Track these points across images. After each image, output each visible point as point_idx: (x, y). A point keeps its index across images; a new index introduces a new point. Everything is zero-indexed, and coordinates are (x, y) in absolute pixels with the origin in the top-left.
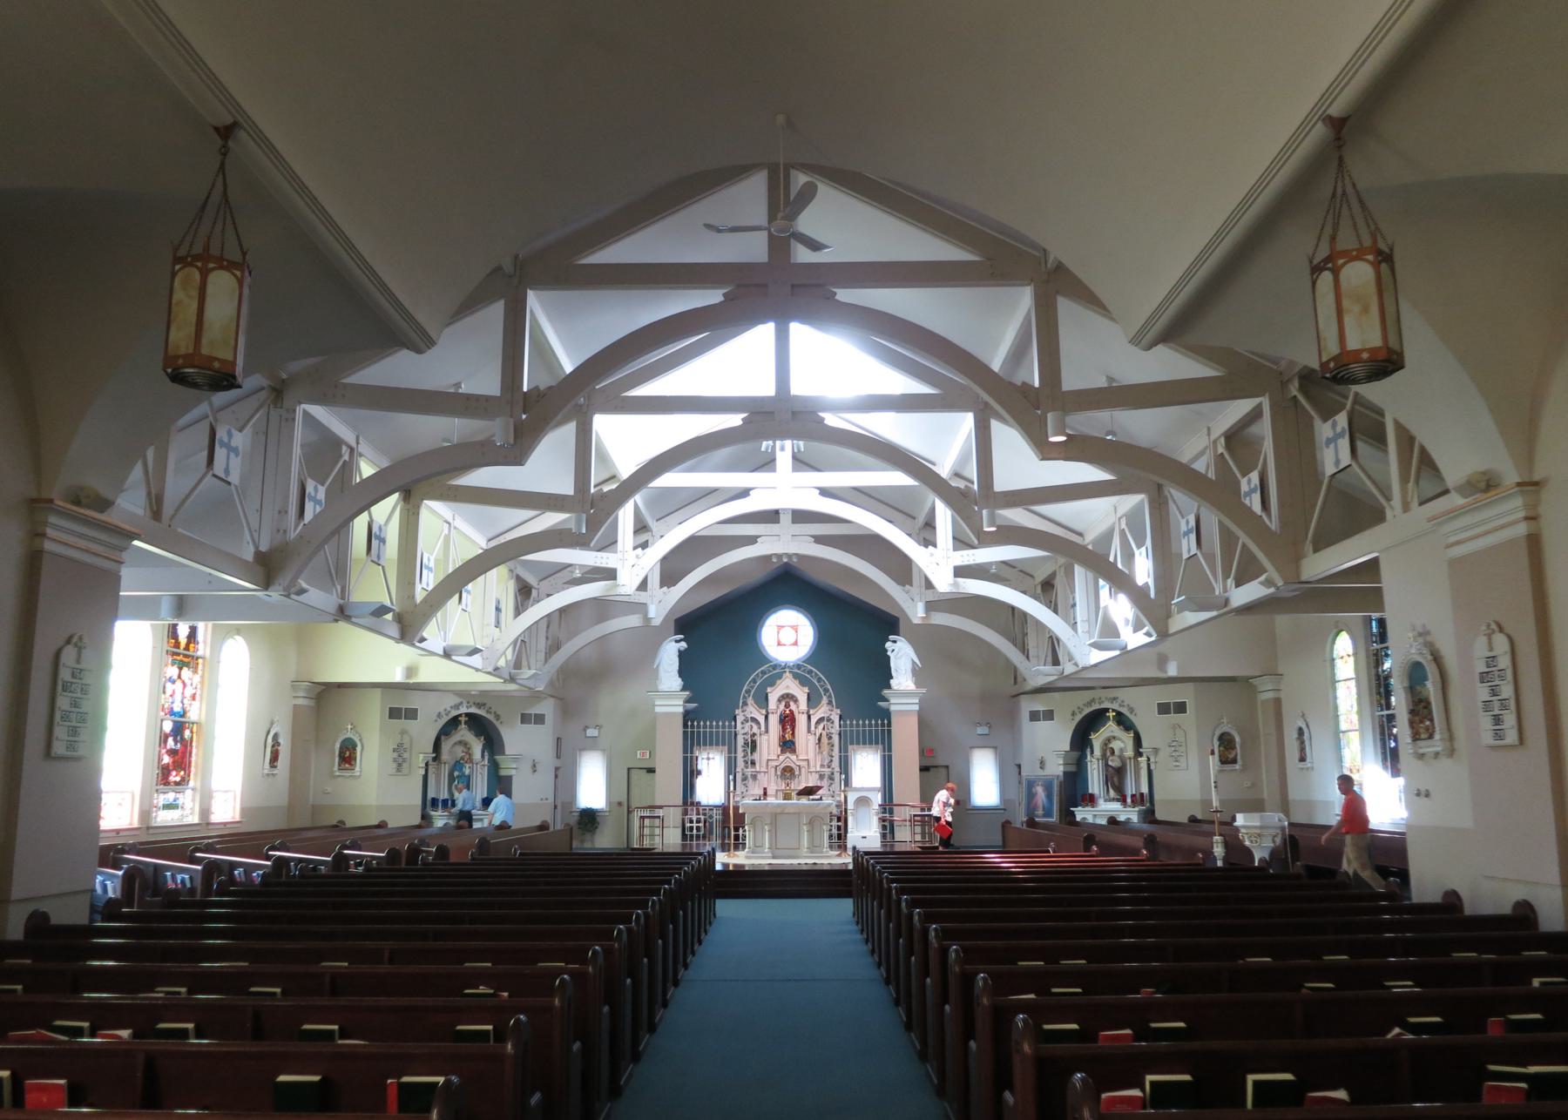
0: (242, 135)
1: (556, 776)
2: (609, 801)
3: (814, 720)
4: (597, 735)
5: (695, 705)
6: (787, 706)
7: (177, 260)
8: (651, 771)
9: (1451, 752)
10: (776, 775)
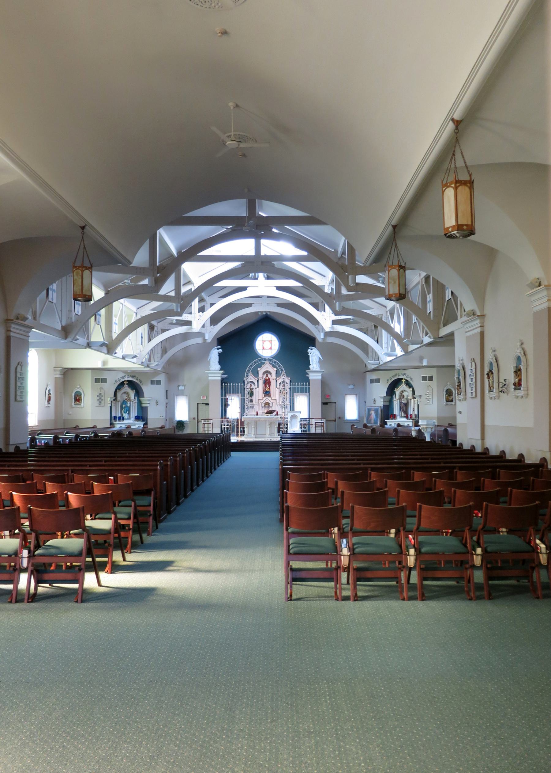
0: (87, 227)
1: (166, 407)
2: (189, 418)
3: (278, 382)
4: (183, 389)
5: (227, 376)
6: (267, 376)
7: (74, 267)
8: (207, 404)
9: (465, 399)
10: (262, 406)
